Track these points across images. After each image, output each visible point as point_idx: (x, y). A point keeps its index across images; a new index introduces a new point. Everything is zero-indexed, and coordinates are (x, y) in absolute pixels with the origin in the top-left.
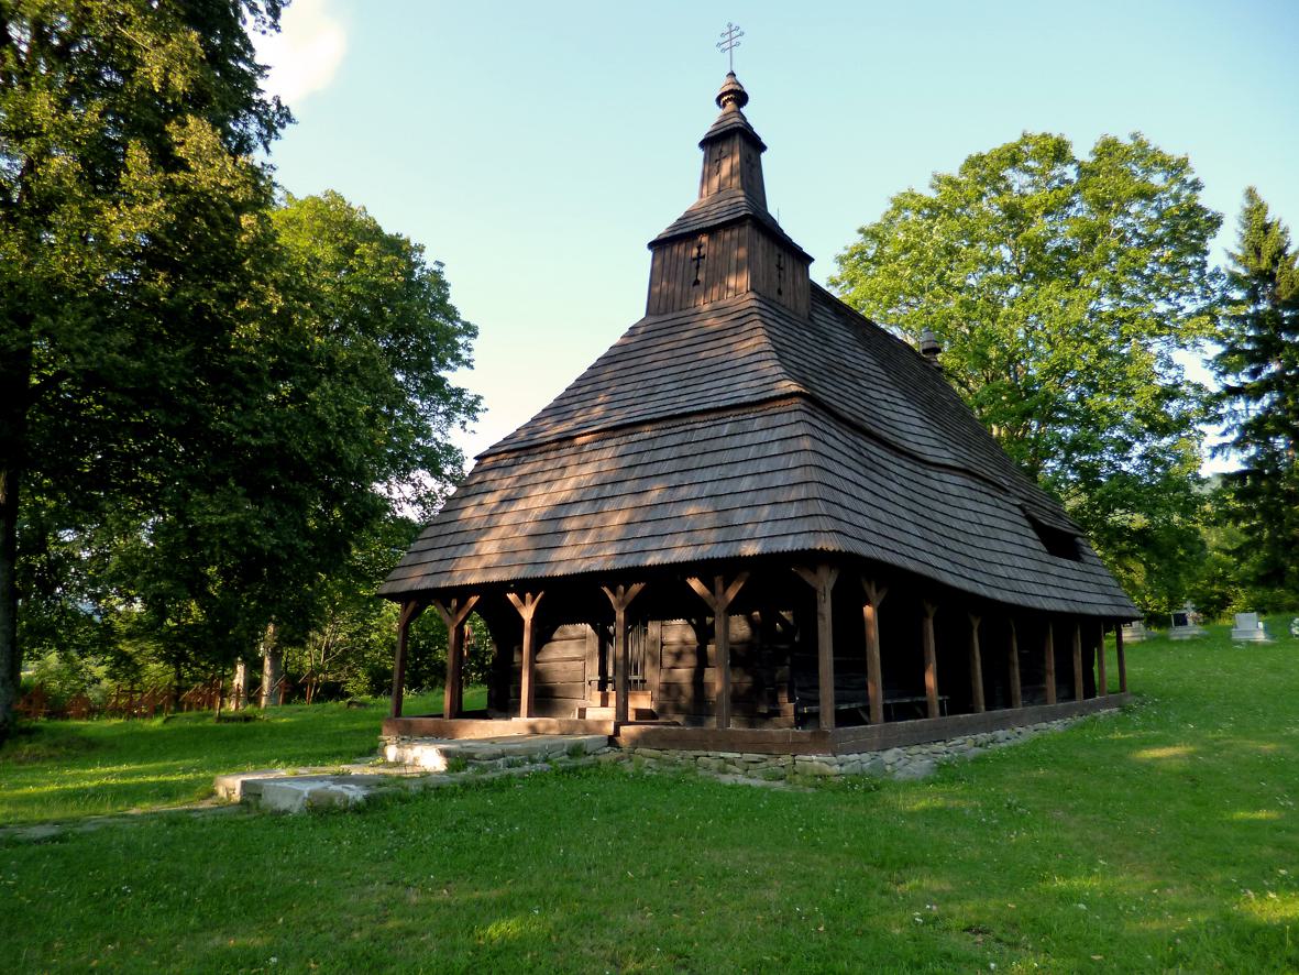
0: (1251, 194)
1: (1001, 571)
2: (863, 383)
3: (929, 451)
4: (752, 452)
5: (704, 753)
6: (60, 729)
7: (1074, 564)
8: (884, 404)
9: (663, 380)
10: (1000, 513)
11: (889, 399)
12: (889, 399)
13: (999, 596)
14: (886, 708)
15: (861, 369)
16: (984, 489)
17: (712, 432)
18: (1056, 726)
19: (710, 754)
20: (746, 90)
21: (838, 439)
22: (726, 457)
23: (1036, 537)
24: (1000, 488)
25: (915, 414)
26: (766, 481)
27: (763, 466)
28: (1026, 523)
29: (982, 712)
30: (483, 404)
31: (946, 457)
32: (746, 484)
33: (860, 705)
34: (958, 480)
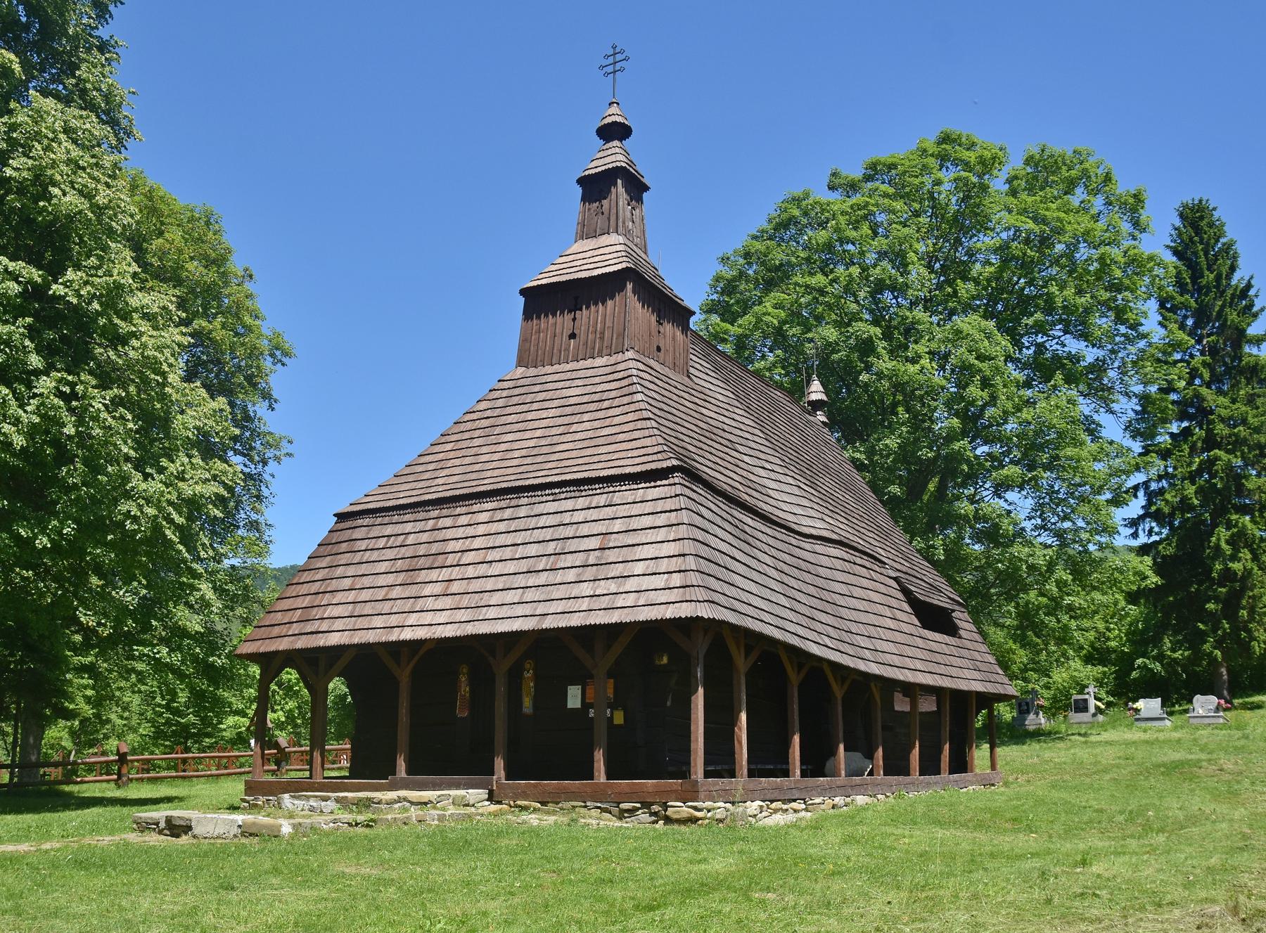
12: (767, 466)
13: (862, 666)
23: (910, 610)
29: (945, 775)
33: (726, 767)
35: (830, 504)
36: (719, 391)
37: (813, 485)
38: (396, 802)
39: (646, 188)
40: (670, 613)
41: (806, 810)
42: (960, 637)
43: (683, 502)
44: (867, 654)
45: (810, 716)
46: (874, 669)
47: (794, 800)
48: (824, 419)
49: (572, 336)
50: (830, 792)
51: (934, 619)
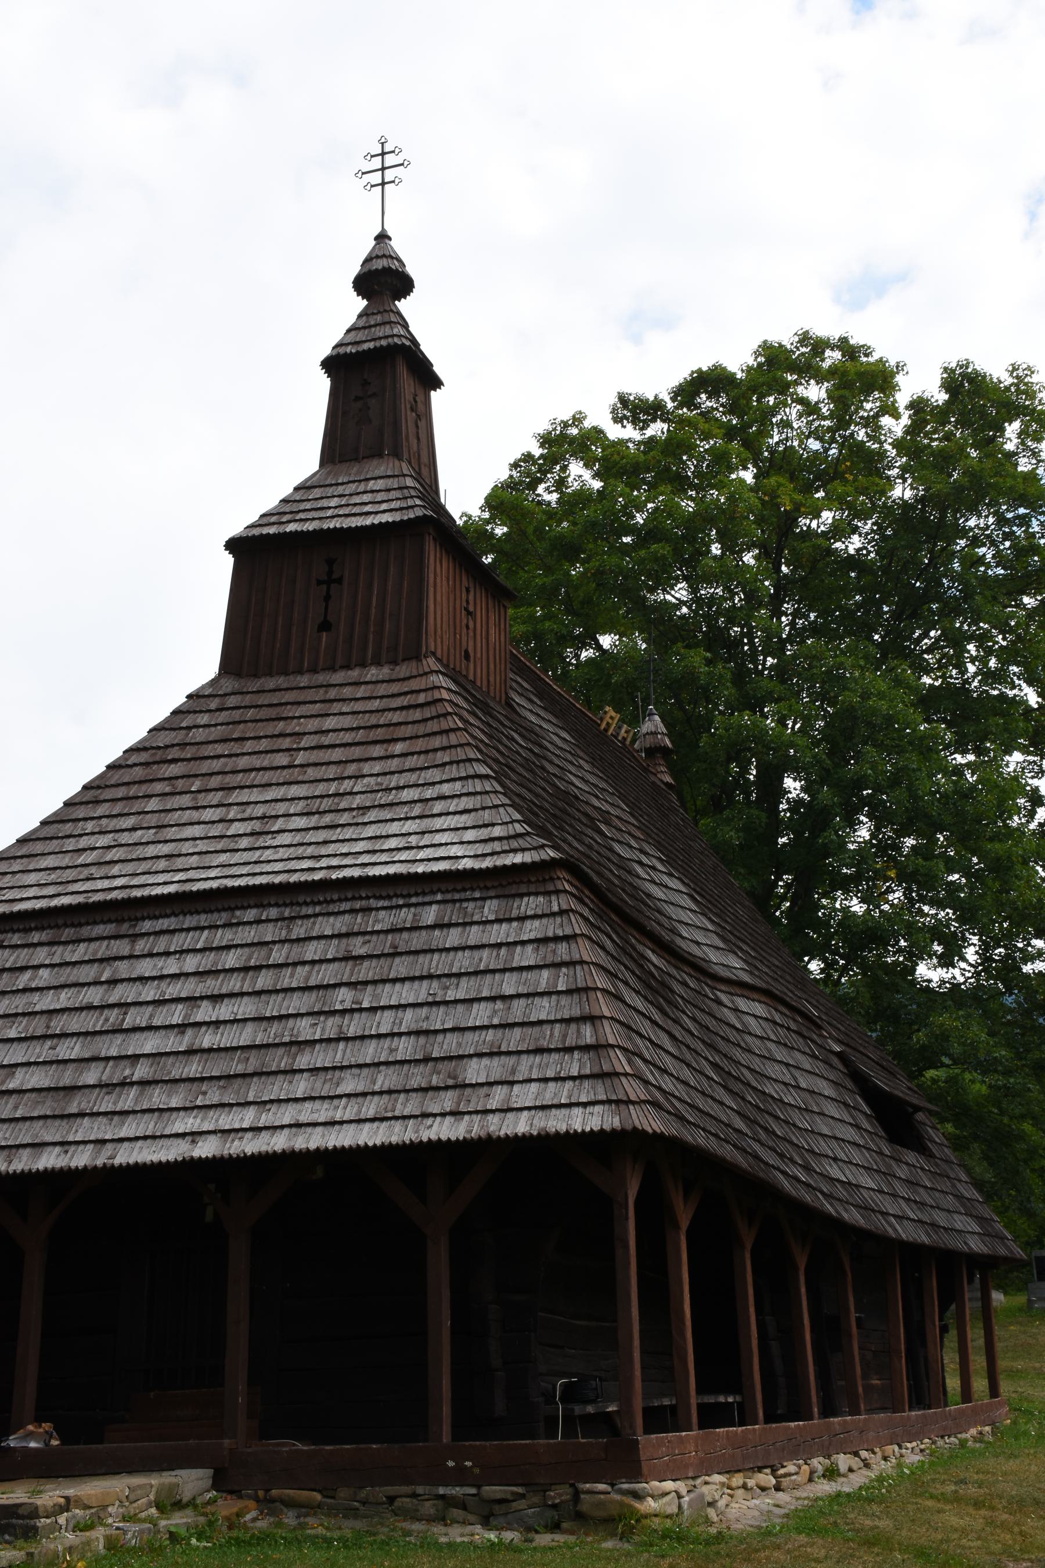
3: (713, 956)
4: (486, 959)
6: (631, 1506)
7: (922, 1161)
9: (281, 808)
14: (647, 1412)
17: (406, 916)
19: (420, 1490)
20: (411, 270)
22: (437, 963)
26: (518, 1011)
27: (509, 985)
28: (850, 1084)
32: (480, 1015)
34: (759, 1009)
39: (436, 383)
40: (557, 1123)
41: (778, 1488)
47: (760, 1469)
48: (668, 779)
49: (325, 626)
50: (800, 1450)
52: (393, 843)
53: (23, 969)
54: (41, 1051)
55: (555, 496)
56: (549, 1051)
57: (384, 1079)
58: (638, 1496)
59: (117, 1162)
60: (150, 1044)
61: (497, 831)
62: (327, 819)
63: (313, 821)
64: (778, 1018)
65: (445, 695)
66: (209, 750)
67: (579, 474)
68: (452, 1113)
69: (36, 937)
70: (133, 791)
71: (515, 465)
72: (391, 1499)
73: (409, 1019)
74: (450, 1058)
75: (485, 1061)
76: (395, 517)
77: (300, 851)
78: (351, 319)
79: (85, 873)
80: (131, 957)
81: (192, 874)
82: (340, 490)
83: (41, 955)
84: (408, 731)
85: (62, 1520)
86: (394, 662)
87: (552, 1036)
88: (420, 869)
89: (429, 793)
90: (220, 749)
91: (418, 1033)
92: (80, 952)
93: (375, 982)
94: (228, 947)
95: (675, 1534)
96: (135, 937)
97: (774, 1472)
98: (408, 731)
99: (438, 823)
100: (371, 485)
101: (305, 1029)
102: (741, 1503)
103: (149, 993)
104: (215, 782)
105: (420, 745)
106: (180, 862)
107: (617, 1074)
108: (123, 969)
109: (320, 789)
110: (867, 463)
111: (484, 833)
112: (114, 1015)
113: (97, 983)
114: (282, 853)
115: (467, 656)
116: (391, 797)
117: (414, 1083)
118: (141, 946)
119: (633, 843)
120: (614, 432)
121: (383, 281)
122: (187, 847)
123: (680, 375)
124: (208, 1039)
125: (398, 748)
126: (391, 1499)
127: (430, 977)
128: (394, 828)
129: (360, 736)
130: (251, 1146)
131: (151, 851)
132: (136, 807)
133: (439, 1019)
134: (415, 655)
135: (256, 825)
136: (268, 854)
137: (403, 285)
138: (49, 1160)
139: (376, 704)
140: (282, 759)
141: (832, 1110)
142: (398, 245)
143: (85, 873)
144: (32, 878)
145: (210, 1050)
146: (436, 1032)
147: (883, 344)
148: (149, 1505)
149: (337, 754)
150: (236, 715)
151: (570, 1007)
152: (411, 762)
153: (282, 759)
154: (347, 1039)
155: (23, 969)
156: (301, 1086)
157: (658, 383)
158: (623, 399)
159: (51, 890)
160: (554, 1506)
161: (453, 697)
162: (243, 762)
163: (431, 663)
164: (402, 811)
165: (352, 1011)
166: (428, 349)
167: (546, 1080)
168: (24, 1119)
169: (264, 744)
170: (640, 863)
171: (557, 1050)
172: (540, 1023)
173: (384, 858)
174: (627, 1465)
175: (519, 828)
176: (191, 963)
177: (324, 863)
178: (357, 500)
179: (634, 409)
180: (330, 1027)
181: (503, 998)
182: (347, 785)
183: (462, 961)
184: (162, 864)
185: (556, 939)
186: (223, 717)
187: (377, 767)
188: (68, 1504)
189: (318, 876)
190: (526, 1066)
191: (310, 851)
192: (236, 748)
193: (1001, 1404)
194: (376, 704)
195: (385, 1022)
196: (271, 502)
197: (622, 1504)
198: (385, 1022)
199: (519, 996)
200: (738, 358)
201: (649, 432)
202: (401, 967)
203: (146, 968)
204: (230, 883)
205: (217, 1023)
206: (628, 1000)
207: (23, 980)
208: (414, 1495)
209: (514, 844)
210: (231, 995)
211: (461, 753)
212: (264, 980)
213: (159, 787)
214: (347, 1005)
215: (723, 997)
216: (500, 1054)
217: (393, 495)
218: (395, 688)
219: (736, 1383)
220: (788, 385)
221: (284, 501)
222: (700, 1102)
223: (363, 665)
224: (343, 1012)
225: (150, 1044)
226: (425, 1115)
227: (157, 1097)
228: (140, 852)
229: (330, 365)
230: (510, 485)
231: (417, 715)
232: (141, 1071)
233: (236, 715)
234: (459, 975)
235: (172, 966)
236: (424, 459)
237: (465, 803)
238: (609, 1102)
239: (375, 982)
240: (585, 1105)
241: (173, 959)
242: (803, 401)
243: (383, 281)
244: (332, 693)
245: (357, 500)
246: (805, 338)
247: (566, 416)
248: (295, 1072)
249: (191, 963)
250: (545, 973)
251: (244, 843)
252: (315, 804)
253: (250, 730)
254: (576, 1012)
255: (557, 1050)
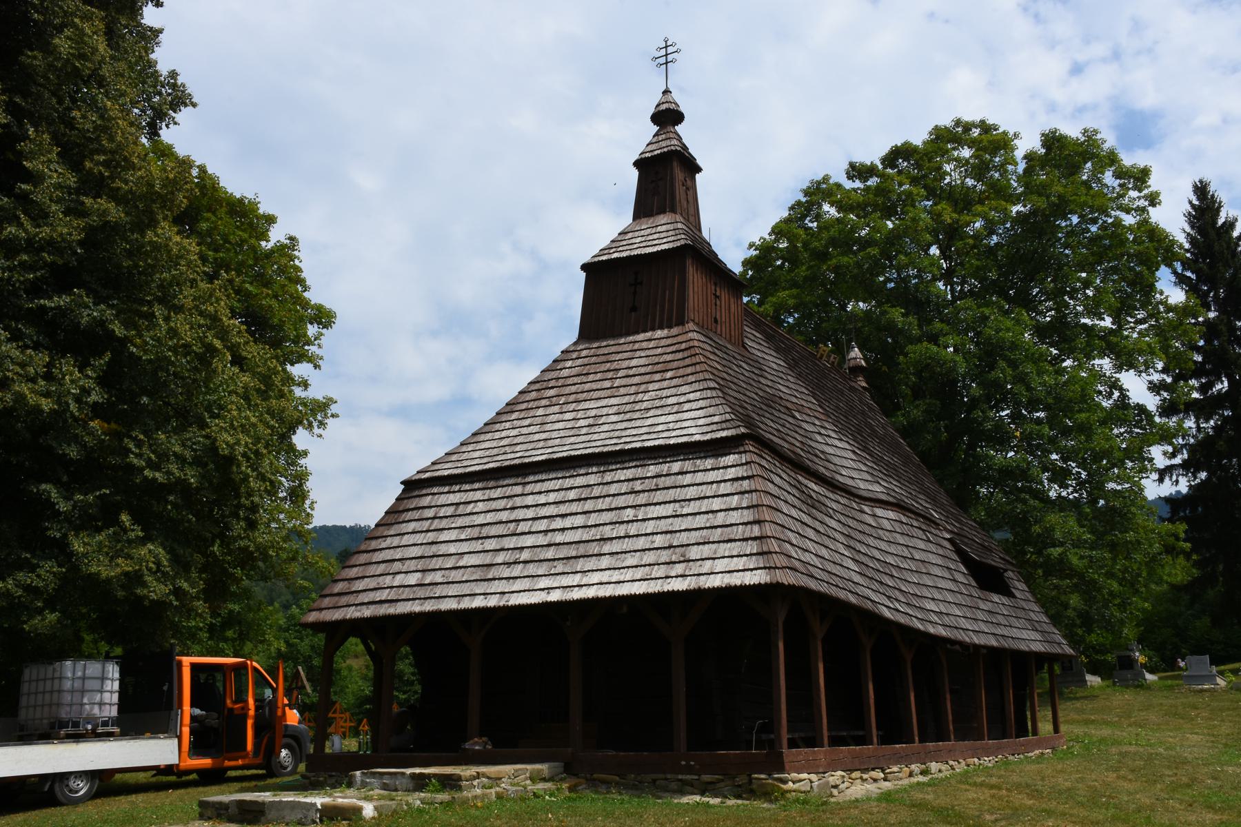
0: (1201, 190)
1: (931, 606)
2: (797, 414)
3: (862, 485)
5: (662, 776)
7: (1005, 600)
8: (819, 438)
9: (605, 411)
10: (933, 548)
11: (823, 431)
15: (794, 400)
16: (915, 524)
17: (664, 468)
18: (988, 761)
19: (669, 776)
20: (682, 109)
21: (782, 479)
24: (929, 520)
25: (848, 447)
28: (955, 557)
30: (334, 409)
31: (877, 490)
34: (891, 515)
35: (890, 471)
36: (773, 362)
37: (865, 449)
38: (475, 778)
39: (699, 170)
40: (736, 580)
41: (885, 779)
42: (1014, 596)
43: (756, 470)
44: (935, 618)
45: (884, 683)
46: (942, 632)
47: (873, 769)
48: (864, 384)
49: (634, 309)
50: (905, 760)
51: (988, 579)
52: (660, 428)
53: (470, 503)
54: (477, 546)
55: (815, 224)
56: (735, 540)
57: (649, 558)
58: (785, 782)
59: (510, 604)
60: (529, 541)
61: (716, 419)
62: (628, 416)
63: (621, 417)
64: (904, 519)
65: (696, 343)
66: (570, 381)
67: (829, 210)
68: (681, 576)
69: (477, 485)
70: (531, 405)
71: (792, 208)
72: (654, 781)
73: (663, 525)
74: (682, 546)
75: (701, 547)
76: (670, 246)
77: (612, 434)
78: (649, 138)
79: (503, 450)
80: (523, 495)
81: (555, 449)
82: (642, 233)
83: (478, 495)
84: (675, 364)
85: (475, 783)
86: (670, 327)
87: (739, 532)
88: (672, 441)
89: (682, 399)
90: (576, 380)
91: (666, 532)
92: (498, 493)
93: (645, 505)
94: (571, 488)
95: (804, 801)
96: (525, 484)
97: (883, 771)
98: (675, 364)
99: (686, 416)
100: (660, 229)
101: (608, 531)
102: (857, 788)
103: (530, 513)
104: (572, 398)
105: (681, 372)
106: (550, 443)
107: (771, 553)
108: (518, 501)
109: (626, 399)
110: (1000, 192)
111: (709, 420)
112: (512, 526)
113: (505, 509)
114: (603, 436)
115: (716, 321)
116: (663, 402)
117: (662, 560)
118: (529, 488)
119: (817, 422)
120: (848, 185)
121: (667, 117)
122: (555, 435)
123: (884, 150)
124: (559, 538)
125: (669, 374)
126: (654, 781)
127: (675, 501)
128: (662, 419)
129: (649, 369)
130: (577, 595)
131: (537, 437)
132: (532, 413)
133: (678, 524)
134: (681, 322)
135: (591, 421)
136: (595, 437)
137: (677, 117)
138: (478, 603)
139: (659, 351)
140: (607, 384)
141: (937, 571)
142: (676, 96)
143: (503, 450)
144: (477, 454)
145: (559, 544)
146: (676, 532)
147: (1005, 122)
148: (526, 779)
149: (636, 380)
150: (586, 361)
151: (748, 516)
152: (675, 382)
153: (607, 384)
154: (629, 537)
155: (470, 503)
156: (605, 562)
157: (873, 154)
158: (852, 166)
159: (485, 460)
160: (739, 786)
161: (701, 345)
162: (587, 387)
163: (691, 326)
164: (667, 410)
165: (632, 521)
166: (693, 151)
167: (732, 557)
168: (467, 581)
169: (599, 376)
170: (820, 433)
171: (739, 540)
172: (732, 525)
173: (654, 436)
174: (776, 764)
175: (728, 417)
176: (552, 497)
177: (623, 440)
178: (651, 237)
179: (858, 171)
180: (621, 530)
181: (712, 512)
182: (640, 397)
183: (692, 492)
184: (541, 444)
185: (743, 478)
186: (579, 362)
187: (657, 386)
188: (478, 776)
189: (618, 448)
190: (724, 549)
191: (617, 434)
192: (584, 379)
193: (1061, 737)
194: (659, 351)
195: (650, 527)
196: (605, 243)
197: (774, 785)
198: (650, 527)
199: (721, 511)
200: (919, 137)
201: (869, 183)
202: (659, 496)
203: (530, 500)
204: (573, 453)
205: (563, 530)
206: (785, 511)
207: (469, 508)
208: (666, 779)
209: (724, 425)
210: (571, 514)
211: (701, 376)
212: (589, 506)
213: (544, 402)
214: (630, 518)
215: (866, 509)
216: (709, 543)
217: (671, 233)
218: (669, 341)
219: (860, 721)
220: (947, 151)
221: (613, 241)
222: (830, 567)
223: (653, 329)
224: (628, 522)
225: (529, 541)
226: (667, 577)
227: (532, 569)
228: (532, 438)
229: (637, 164)
230: (787, 221)
231: (680, 355)
232: (525, 555)
233: (586, 361)
234: (690, 500)
235: (542, 499)
236: (692, 211)
237: (701, 404)
238: (765, 568)
239: (645, 505)
240: (751, 570)
241: (545, 493)
242: (958, 160)
243: (667, 117)
244: (637, 346)
245: (651, 237)
246: (958, 122)
247: (819, 177)
248: (601, 555)
249: (552, 497)
250: (736, 497)
251: (584, 431)
252: (623, 408)
253: (592, 369)
254: (751, 519)
255: (739, 540)
